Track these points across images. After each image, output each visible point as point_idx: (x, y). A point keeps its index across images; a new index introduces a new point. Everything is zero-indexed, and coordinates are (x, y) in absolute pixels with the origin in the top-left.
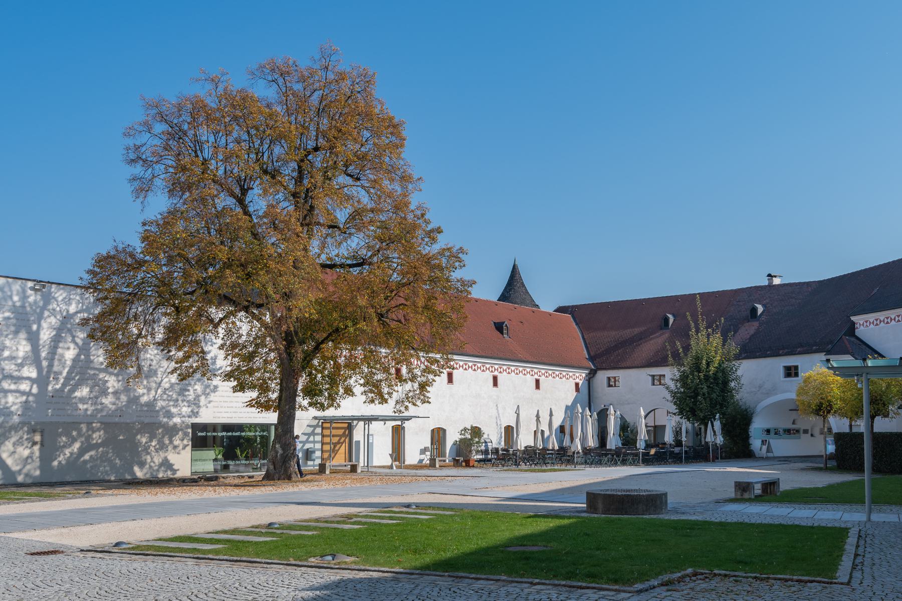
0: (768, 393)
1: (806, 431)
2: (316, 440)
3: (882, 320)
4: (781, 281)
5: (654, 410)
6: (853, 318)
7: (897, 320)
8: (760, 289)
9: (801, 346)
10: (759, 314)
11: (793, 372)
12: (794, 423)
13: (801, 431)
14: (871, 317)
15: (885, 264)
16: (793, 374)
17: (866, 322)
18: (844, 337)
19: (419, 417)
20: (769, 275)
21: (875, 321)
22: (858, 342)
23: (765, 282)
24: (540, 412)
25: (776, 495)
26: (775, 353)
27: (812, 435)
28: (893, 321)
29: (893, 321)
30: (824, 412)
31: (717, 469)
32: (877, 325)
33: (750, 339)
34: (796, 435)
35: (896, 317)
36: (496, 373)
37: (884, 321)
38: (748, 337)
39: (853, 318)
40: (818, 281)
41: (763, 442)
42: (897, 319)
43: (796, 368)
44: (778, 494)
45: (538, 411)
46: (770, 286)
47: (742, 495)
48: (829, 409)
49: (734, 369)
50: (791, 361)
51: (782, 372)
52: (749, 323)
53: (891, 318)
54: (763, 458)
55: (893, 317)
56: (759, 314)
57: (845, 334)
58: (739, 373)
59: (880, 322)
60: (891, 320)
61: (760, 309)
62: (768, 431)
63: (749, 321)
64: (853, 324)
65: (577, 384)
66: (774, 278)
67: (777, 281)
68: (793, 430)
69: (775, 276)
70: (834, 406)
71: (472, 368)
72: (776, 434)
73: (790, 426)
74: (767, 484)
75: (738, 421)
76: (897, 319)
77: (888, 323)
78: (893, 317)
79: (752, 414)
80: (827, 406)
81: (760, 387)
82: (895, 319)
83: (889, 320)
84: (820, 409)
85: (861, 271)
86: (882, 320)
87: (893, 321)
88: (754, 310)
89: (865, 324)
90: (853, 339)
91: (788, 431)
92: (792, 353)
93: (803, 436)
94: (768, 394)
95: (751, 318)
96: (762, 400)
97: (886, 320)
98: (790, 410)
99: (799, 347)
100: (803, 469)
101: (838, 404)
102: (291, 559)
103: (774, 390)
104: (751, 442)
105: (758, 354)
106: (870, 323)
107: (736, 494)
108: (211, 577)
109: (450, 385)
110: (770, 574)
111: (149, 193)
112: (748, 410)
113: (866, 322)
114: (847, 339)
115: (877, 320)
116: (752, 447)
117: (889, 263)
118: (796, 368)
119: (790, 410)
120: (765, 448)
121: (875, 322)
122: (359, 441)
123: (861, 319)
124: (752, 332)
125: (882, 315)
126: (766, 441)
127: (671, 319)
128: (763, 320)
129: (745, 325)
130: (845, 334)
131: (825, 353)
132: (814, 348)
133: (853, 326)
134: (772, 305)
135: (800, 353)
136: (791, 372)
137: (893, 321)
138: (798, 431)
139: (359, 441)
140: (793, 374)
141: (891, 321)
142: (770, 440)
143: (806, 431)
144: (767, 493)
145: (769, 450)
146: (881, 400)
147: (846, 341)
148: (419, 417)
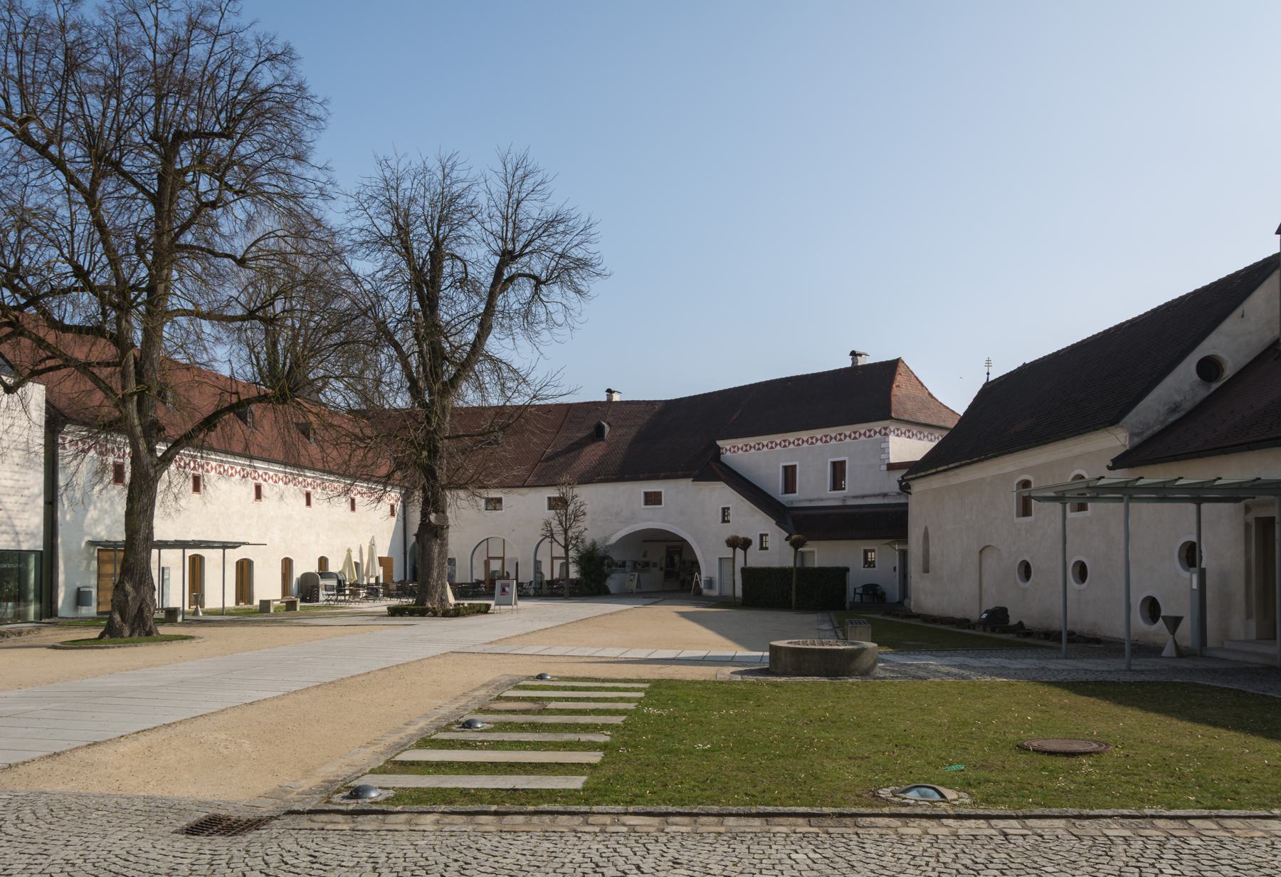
3: (862, 437)
6: (719, 443)
12: (644, 556)
14: (740, 442)
19: (249, 544)
21: (828, 440)
23: (604, 398)
24: (930, 531)
29: (848, 438)
31: (890, 619)
32: (746, 451)
37: (754, 447)
39: (719, 443)
42: (770, 446)
43: (659, 494)
45: (926, 528)
46: (610, 402)
50: (653, 486)
59: (751, 447)
64: (719, 448)
67: (616, 398)
71: (742, 449)
76: (770, 446)
77: (759, 449)
86: (862, 437)
87: (848, 438)
98: (644, 541)
108: (22, 833)
109: (258, 502)
113: (734, 447)
118: (659, 494)
119: (644, 541)
123: (728, 444)
127: (607, 429)
136: (653, 499)
148: (249, 544)
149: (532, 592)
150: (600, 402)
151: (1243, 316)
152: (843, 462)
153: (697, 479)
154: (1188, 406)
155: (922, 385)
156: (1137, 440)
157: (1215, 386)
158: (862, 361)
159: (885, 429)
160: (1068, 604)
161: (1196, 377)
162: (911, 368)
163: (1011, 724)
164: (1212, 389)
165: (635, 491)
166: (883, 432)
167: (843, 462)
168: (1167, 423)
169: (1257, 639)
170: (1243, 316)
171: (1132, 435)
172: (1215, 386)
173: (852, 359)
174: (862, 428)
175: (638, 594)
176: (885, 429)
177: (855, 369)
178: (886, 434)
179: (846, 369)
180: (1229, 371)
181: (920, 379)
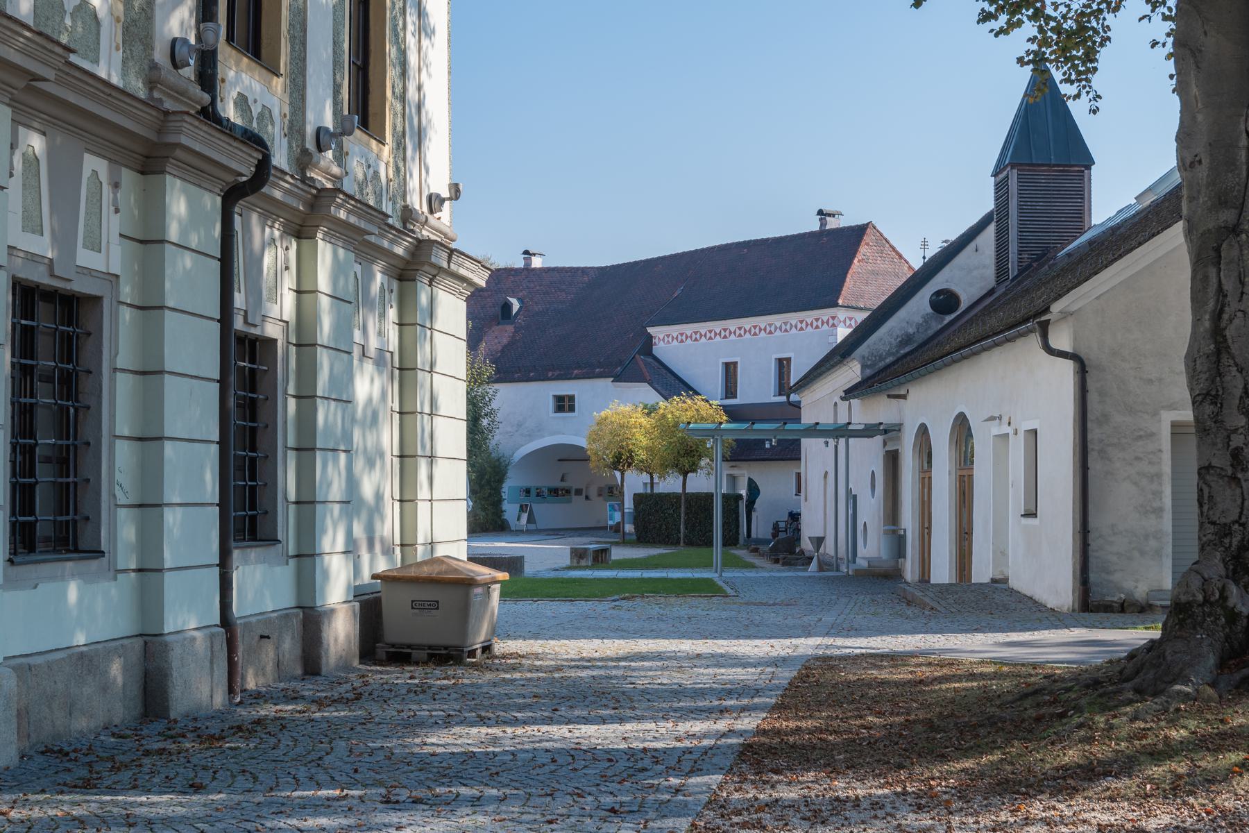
0: (529, 435)
1: (579, 492)
2: (118, 443)
4: (543, 263)
6: (650, 330)
7: (708, 337)
8: (513, 272)
9: (579, 367)
10: (514, 312)
11: (567, 404)
12: (562, 480)
13: (573, 492)
14: (675, 330)
15: (690, 252)
16: (567, 407)
17: (668, 336)
18: (637, 356)
20: (526, 252)
21: (757, 332)
22: (656, 364)
23: (519, 263)
25: (608, 563)
26: (541, 375)
27: (587, 498)
28: (703, 334)
30: (623, 466)
31: (483, 545)
32: (682, 341)
33: (502, 351)
34: (566, 497)
35: (820, 326)
38: (500, 348)
39: (650, 330)
40: (598, 268)
41: (523, 508)
42: (788, 326)
43: (572, 398)
44: (610, 562)
46: (528, 270)
47: (578, 563)
48: (630, 461)
49: (487, 399)
51: (551, 404)
52: (500, 326)
54: (522, 531)
55: (825, 319)
56: (514, 312)
57: (639, 353)
58: (494, 405)
59: (828, 322)
60: (701, 336)
61: (516, 305)
62: (528, 491)
63: (498, 324)
64: (650, 337)
66: (533, 258)
67: (537, 263)
68: (562, 490)
69: (534, 255)
70: (636, 458)
72: (538, 495)
73: (557, 484)
74: (598, 551)
75: (487, 477)
78: (825, 319)
79: (507, 465)
80: (628, 458)
81: (519, 425)
82: (705, 336)
83: (698, 336)
84: (619, 462)
85: (659, 258)
87: (661, 338)
88: (507, 307)
89: (666, 339)
90: (650, 360)
91: (554, 492)
93: (574, 498)
94: (531, 436)
95: (502, 319)
96: (517, 449)
97: (804, 325)
98: (559, 460)
99: (576, 368)
101: (642, 455)
103: (539, 431)
104: (504, 508)
105: (516, 376)
106: (673, 337)
107: (571, 562)
110: (338, 799)
112: (501, 460)
113: (668, 336)
114: (643, 360)
116: (506, 516)
117: (696, 251)
118: (572, 398)
119: (559, 460)
120: (525, 516)
121: (680, 338)
124: (505, 341)
125: (688, 329)
126: (527, 506)
128: (520, 323)
129: (493, 329)
130: (639, 353)
131: (612, 379)
132: (597, 370)
133: (649, 341)
134: (531, 299)
135: (577, 377)
136: (564, 404)
137: (703, 334)
138: (568, 492)
140: (567, 407)
141: (701, 338)
142: (533, 505)
143: (579, 492)
144: (598, 561)
145: (531, 520)
146: (697, 451)
147: (642, 365)
149: (491, 527)
150: (512, 270)
151: (977, 250)
152: (735, 364)
153: (618, 378)
154: (920, 339)
155: (901, 256)
156: (869, 372)
157: (948, 318)
158: (832, 224)
159: (833, 318)
160: (839, 545)
161: (929, 310)
162: (886, 235)
163: (933, 704)
164: (946, 322)
165: (546, 391)
166: (831, 322)
167: (735, 364)
168: (899, 355)
169: (919, 581)
170: (977, 250)
171: (864, 367)
172: (948, 318)
173: (821, 219)
174: (809, 316)
175: (528, 532)
176: (833, 318)
177: (823, 233)
178: (834, 325)
179: (812, 234)
180: (963, 306)
181: (898, 249)
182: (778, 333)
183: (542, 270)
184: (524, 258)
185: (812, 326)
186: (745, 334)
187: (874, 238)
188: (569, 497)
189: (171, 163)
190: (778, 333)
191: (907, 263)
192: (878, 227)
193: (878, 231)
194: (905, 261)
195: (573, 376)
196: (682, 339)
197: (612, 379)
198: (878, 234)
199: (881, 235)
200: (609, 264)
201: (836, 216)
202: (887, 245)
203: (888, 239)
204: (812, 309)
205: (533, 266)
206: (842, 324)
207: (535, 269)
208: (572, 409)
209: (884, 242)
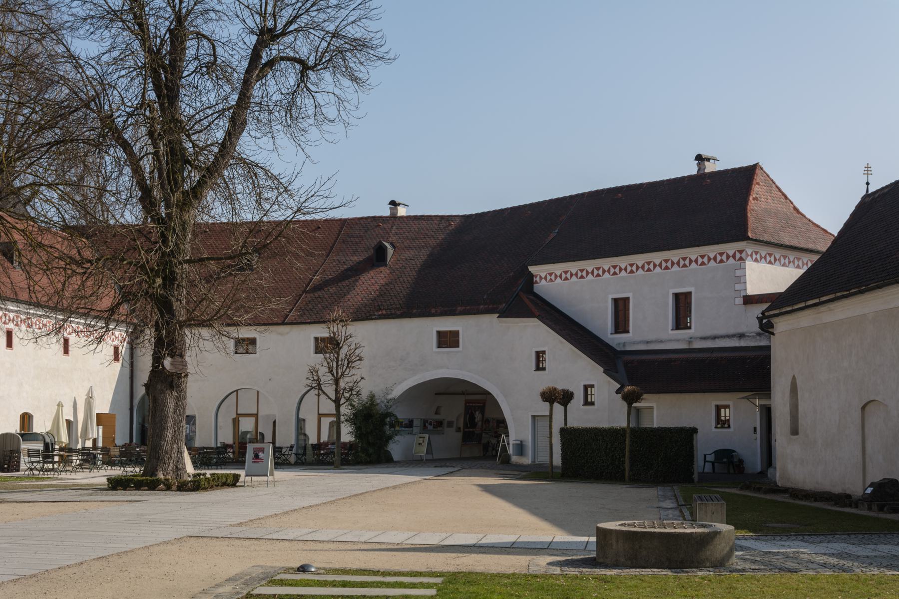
5: (237, 391)
6: (532, 269)
7: (595, 274)
12: (436, 413)
13: (445, 424)
14: (558, 268)
23: (386, 212)
28: (558, 278)
29: (574, 277)
36: (11, 326)
39: (532, 269)
43: (456, 334)
46: (394, 217)
50: (448, 324)
53: (715, 261)
64: (531, 276)
65: (116, 349)
67: (402, 212)
78: (712, 256)
86: (590, 271)
92: (448, 311)
98: (436, 394)
100: (743, 398)
102: (208, 476)
111: (325, 80)
115: (566, 272)
118: (456, 334)
122: (440, 334)
127: (390, 251)
131: (498, 315)
132: (482, 307)
133: (530, 279)
136: (448, 340)
137: (558, 278)
139: (440, 334)
155: (786, 197)
158: (710, 167)
166: (738, 255)
167: (688, 295)
173: (698, 165)
176: (741, 252)
178: (741, 259)
182: (676, 268)
183: (408, 218)
184: (390, 208)
185: (715, 261)
186: (679, 261)
187: (762, 178)
188: (441, 428)
189: (104, 485)
190: (676, 268)
191: (792, 203)
192: (765, 169)
193: (765, 172)
194: (790, 201)
195: (457, 312)
196: (567, 276)
197: (498, 315)
198: (765, 175)
199: (768, 176)
200: (474, 213)
201: (711, 161)
202: (774, 186)
203: (774, 180)
204: (718, 243)
205: (399, 215)
206: (749, 257)
207: (402, 217)
208: (456, 344)
209: (771, 182)
